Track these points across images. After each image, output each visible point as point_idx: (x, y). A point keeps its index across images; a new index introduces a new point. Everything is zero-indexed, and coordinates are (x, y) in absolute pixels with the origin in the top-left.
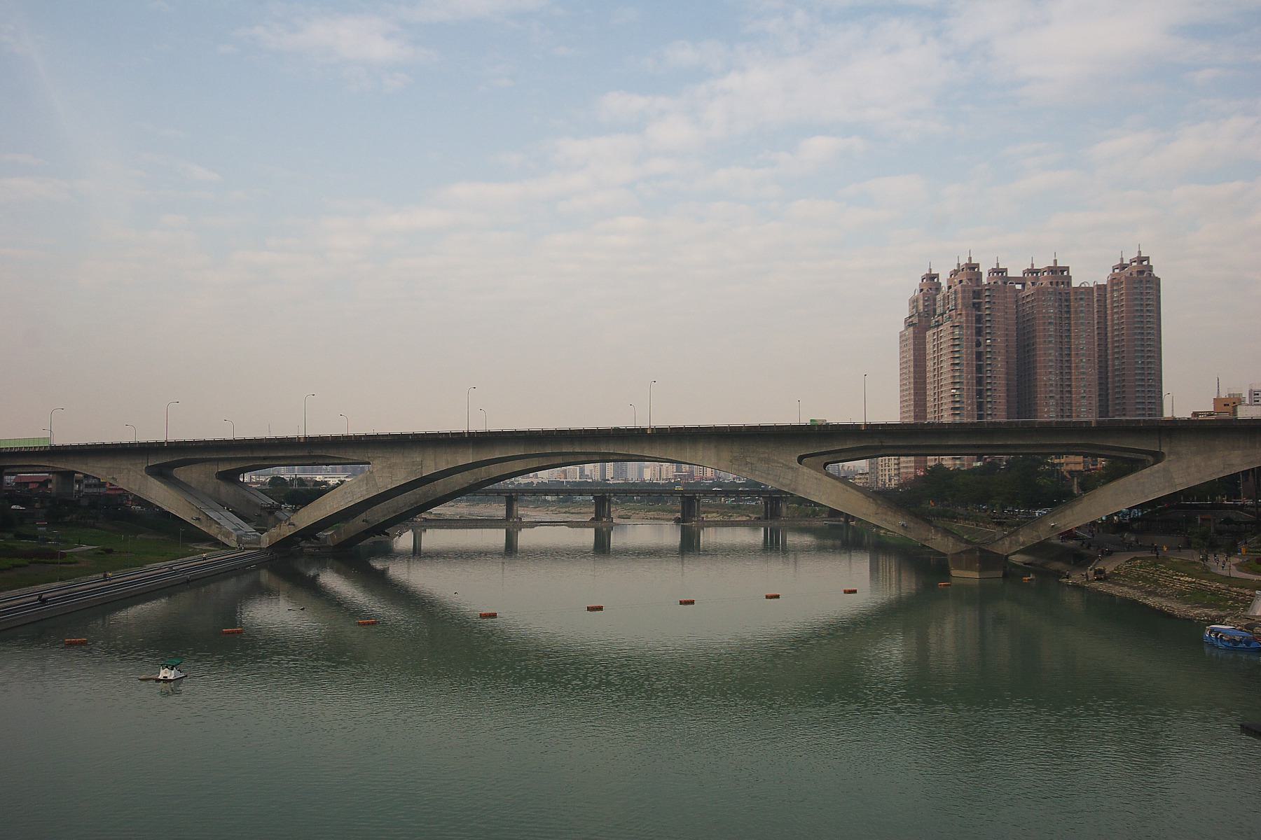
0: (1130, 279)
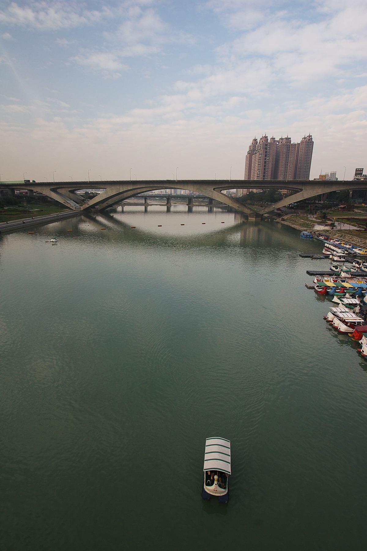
0: (306, 142)
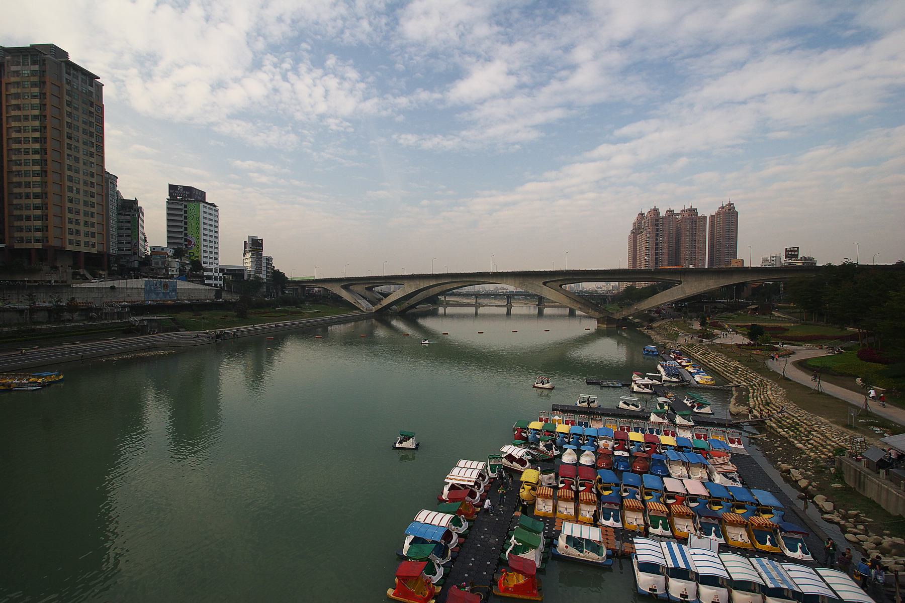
0: (725, 213)
